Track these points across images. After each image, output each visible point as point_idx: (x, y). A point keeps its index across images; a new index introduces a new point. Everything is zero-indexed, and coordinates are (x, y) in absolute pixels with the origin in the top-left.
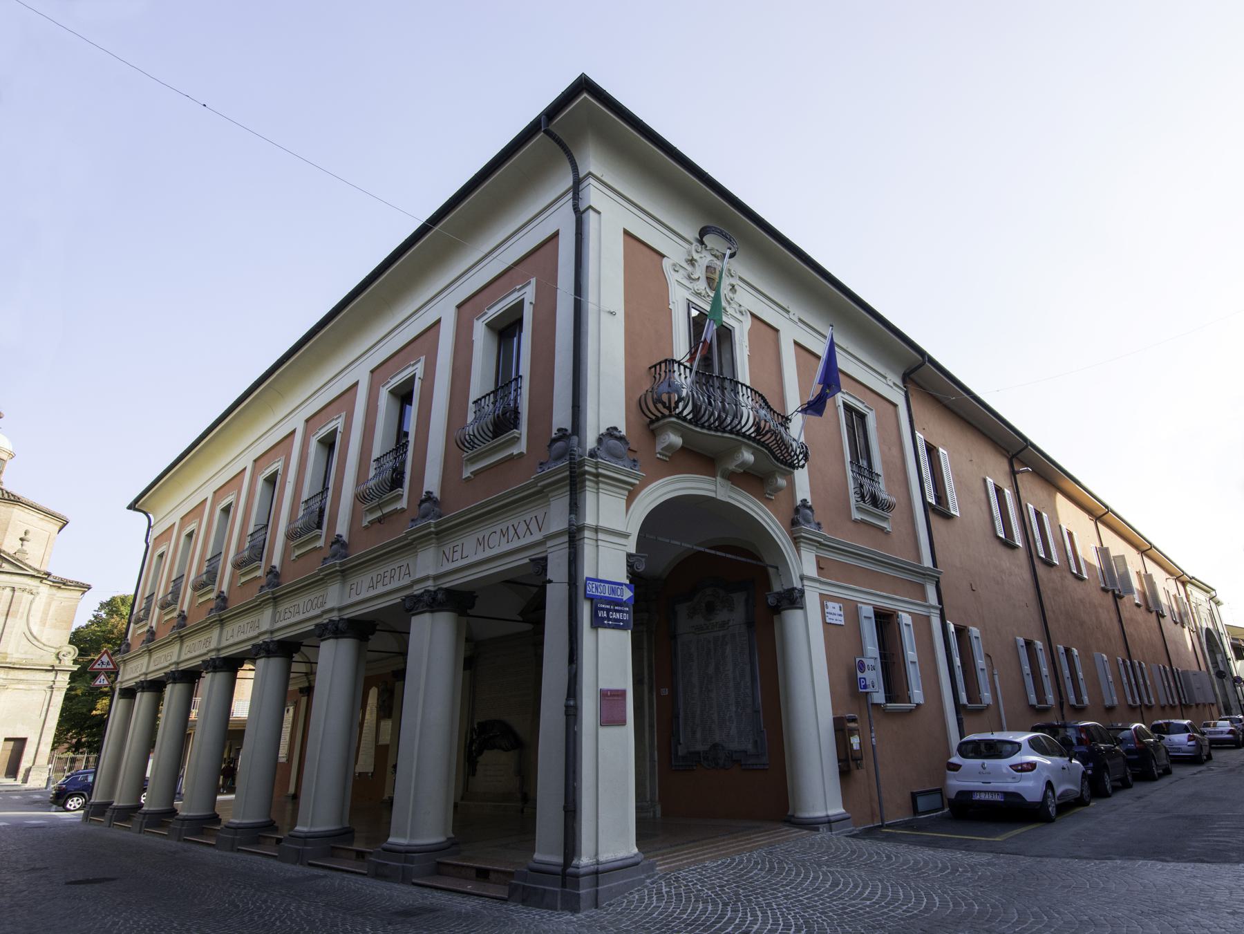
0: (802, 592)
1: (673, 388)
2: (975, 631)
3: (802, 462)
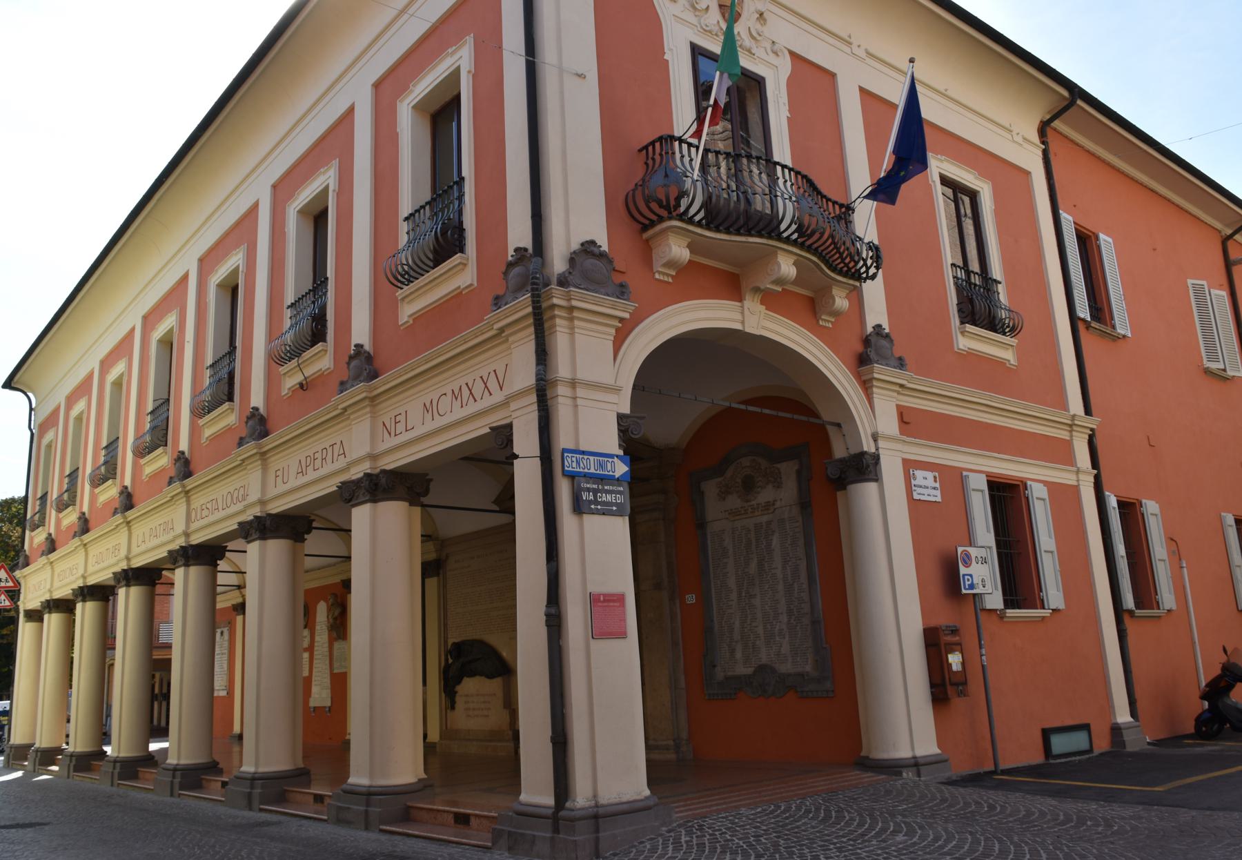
0: (876, 458)
1: (674, 178)
2: (1151, 508)
3: (872, 271)
